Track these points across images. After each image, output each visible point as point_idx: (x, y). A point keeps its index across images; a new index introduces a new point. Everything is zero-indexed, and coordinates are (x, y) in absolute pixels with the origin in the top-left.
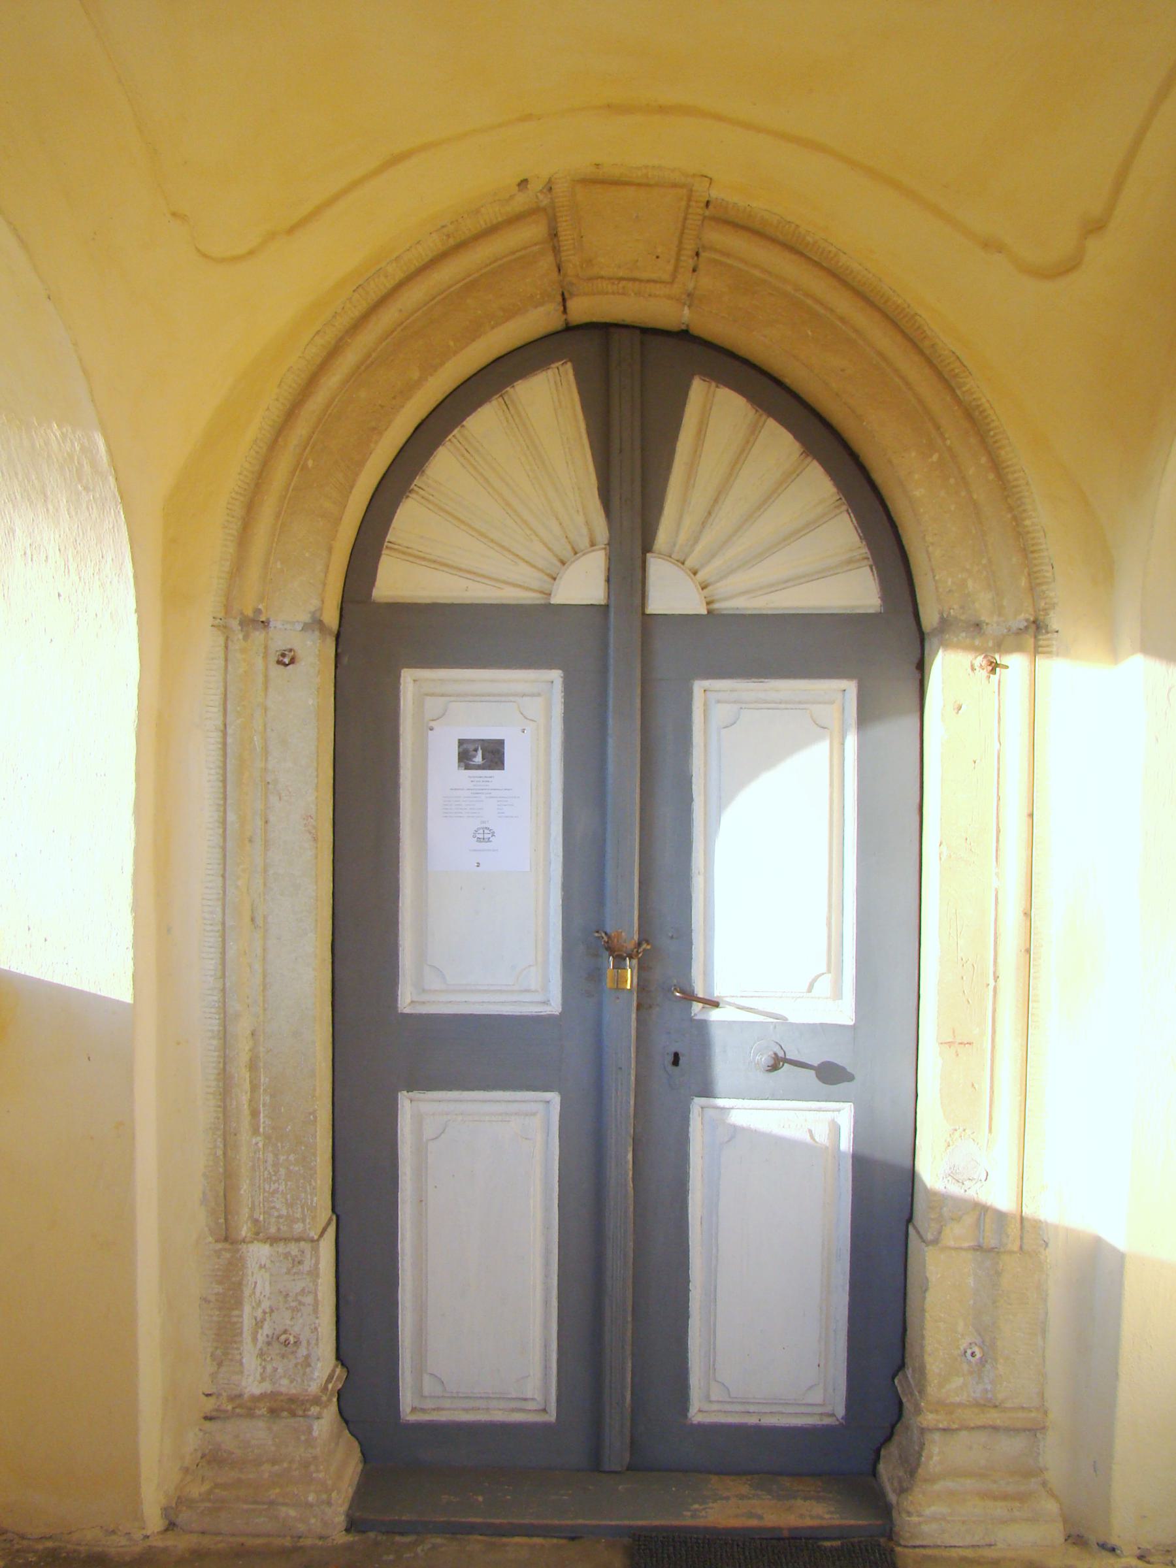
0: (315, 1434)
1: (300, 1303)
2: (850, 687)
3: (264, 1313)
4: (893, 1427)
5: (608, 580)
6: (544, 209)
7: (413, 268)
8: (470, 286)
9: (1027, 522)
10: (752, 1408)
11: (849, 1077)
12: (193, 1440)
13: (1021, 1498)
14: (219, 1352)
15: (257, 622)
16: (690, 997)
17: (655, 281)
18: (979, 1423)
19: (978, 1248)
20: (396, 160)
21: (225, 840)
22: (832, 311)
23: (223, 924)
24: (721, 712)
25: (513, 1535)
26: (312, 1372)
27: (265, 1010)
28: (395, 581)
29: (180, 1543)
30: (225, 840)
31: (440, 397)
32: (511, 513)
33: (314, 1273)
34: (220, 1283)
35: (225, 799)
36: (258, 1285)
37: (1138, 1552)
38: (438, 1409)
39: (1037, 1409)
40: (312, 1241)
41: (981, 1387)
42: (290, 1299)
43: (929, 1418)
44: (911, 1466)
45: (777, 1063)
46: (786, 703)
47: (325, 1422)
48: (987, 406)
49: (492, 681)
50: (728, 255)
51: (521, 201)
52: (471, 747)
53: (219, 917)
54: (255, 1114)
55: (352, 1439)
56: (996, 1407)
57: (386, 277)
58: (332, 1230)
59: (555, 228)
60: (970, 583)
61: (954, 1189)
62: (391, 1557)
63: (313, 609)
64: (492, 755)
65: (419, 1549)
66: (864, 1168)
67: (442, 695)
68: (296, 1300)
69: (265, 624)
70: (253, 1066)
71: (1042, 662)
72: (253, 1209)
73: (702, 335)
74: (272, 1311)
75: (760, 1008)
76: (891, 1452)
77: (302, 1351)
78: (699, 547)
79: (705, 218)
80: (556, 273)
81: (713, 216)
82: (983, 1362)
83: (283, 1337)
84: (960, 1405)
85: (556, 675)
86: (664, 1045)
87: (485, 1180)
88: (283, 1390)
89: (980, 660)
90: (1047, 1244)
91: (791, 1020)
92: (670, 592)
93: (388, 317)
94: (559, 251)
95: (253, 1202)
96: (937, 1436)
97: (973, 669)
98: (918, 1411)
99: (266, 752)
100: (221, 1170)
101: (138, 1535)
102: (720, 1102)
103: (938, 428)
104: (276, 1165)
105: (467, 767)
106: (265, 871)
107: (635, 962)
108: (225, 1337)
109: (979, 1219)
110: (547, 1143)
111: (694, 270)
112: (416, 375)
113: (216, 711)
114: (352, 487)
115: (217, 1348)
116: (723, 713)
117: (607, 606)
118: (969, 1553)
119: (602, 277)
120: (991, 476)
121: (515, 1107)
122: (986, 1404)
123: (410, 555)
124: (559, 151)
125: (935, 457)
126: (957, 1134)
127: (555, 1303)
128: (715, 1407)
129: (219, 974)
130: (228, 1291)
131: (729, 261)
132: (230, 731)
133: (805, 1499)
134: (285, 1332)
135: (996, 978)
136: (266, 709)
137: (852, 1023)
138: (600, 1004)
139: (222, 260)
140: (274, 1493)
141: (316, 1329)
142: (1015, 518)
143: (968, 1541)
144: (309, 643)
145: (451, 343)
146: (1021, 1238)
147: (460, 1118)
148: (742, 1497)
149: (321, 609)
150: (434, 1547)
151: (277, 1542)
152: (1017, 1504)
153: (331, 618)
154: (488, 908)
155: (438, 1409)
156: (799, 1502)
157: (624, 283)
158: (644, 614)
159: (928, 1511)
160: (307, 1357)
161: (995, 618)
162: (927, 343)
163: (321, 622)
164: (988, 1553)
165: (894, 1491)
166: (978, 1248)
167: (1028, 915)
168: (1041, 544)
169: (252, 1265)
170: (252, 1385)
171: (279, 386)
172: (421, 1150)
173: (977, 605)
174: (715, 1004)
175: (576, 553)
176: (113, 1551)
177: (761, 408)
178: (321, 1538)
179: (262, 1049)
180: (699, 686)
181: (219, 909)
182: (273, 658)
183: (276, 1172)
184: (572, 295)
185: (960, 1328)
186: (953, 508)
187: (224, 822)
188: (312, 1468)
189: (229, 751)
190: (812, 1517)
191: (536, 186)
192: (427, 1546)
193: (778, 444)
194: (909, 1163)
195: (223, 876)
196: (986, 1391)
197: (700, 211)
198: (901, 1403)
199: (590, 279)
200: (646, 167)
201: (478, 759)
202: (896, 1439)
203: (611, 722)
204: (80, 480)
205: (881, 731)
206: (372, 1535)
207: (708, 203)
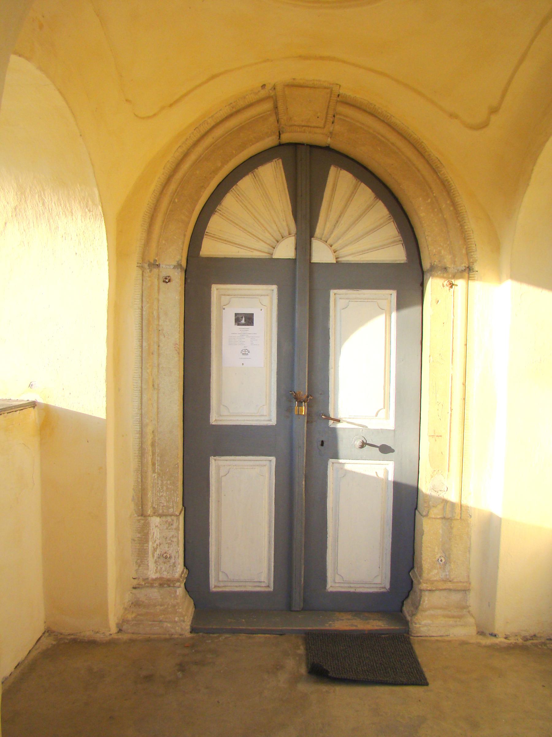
0: (178, 594)
1: (172, 541)
2: (394, 293)
3: (157, 545)
4: (409, 592)
5: (296, 249)
6: (272, 97)
7: (218, 121)
8: (241, 128)
9: (466, 227)
10: (352, 585)
11: (393, 451)
12: (128, 597)
13: (460, 617)
14: (139, 561)
15: (155, 265)
16: (328, 418)
17: (317, 127)
18: (444, 588)
19: (444, 518)
20: (213, 77)
21: (142, 354)
22: (388, 140)
23: (141, 387)
24: (341, 303)
25: (258, 634)
26: (176, 569)
27: (158, 422)
28: (209, 248)
29: (125, 637)
30: (142, 354)
31: (227, 173)
32: (255, 220)
33: (177, 529)
34: (139, 533)
35: (142, 337)
36: (155, 534)
37: (504, 636)
38: (225, 586)
39: (466, 582)
40: (177, 516)
41: (444, 574)
42: (168, 539)
43: (424, 586)
44: (416, 606)
45: (363, 445)
46: (368, 299)
47: (180, 591)
48: (450, 180)
49: (248, 289)
50: (346, 117)
51: (263, 93)
52: (240, 316)
53: (140, 385)
54: (154, 464)
55: (190, 598)
56: (450, 581)
57: (208, 124)
58: (183, 512)
59: (277, 105)
60: (442, 252)
61: (434, 494)
62: (210, 641)
63: (178, 260)
64: (249, 320)
65: (221, 638)
66: (398, 487)
67: (229, 295)
68: (170, 540)
69: (158, 266)
70: (153, 445)
71: (471, 283)
72: (153, 503)
73: (335, 148)
74: (160, 544)
75: (357, 423)
76: (409, 601)
77: (173, 561)
78: (333, 236)
79: (337, 102)
80: (276, 123)
81: (339, 102)
82: (445, 563)
83: (165, 555)
84: (436, 581)
85: (275, 287)
86: (317, 438)
87: (245, 492)
88: (165, 576)
89: (446, 283)
90: (471, 516)
91: (369, 427)
92: (321, 254)
93: (209, 140)
94: (278, 114)
95: (153, 500)
96: (427, 593)
97: (444, 286)
98: (419, 583)
99: (159, 318)
100: (140, 487)
101: (107, 634)
102: (341, 461)
103: (431, 188)
104: (162, 485)
105: (238, 325)
106: (158, 365)
107: (306, 404)
108: (141, 555)
109: (444, 507)
110: (270, 479)
111: (333, 123)
112: (219, 165)
113: (138, 301)
114: (193, 210)
115: (138, 559)
116: (343, 304)
117: (295, 259)
118: (439, 638)
119: (295, 125)
120: (452, 208)
121: (258, 463)
122: (446, 580)
123: (216, 238)
124: (279, 74)
125: (429, 200)
126: (435, 473)
127: (273, 552)
128: (337, 585)
129: (140, 408)
130: (143, 536)
131: (347, 119)
132: (144, 309)
133: (374, 620)
134: (166, 553)
135: (451, 410)
136: (158, 300)
137: (393, 429)
138: (292, 421)
139: (143, 118)
140: (161, 617)
141: (178, 551)
142: (461, 225)
143: (439, 633)
144: (176, 274)
145: (234, 152)
146: (461, 514)
147: (235, 467)
148: (349, 619)
149: (181, 260)
150: (226, 638)
151: (163, 636)
152: (458, 620)
153: (184, 264)
154: (247, 380)
155: (225, 586)
156: (371, 621)
157: (304, 128)
158: (310, 262)
159: (423, 622)
160: (174, 563)
161: (453, 266)
162: (426, 153)
163: (181, 265)
164: (447, 638)
165: (409, 616)
166: (444, 518)
167: (464, 384)
168: (470, 236)
169: (152, 526)
170: (152, 574)
171: (164, 168)
172: (219, 481)
173: (445, 260)
174: (339, 421)
175: (283, 238)
176: (98, 639)
177: (359, 179)
178: (180, 635)
179: (157, 438)
180: (332, 292)
181: (140, 382)
182: (161, 280)
183: (162, 488)
184: (283, 132)
185: (436, 550)
186: (436, 221)
187: (142, 346)
188: (177, 607)
189: (144, 317)
190: (377, 626)
191: (269, 87)
192: (223, 638)
193: (365, 194)
194: (416, 484)
195: (142, 368)
196: (446, 575)
197: (336, 99)
198: (412, 582)
199: (291, 126)
200: (314, 80)
201: (243, 321)
202: (410, 596)
203: (297, 306)
204: (87, 207)
205: (406, 312)
206: (201, 634)
207: (339, 95)
